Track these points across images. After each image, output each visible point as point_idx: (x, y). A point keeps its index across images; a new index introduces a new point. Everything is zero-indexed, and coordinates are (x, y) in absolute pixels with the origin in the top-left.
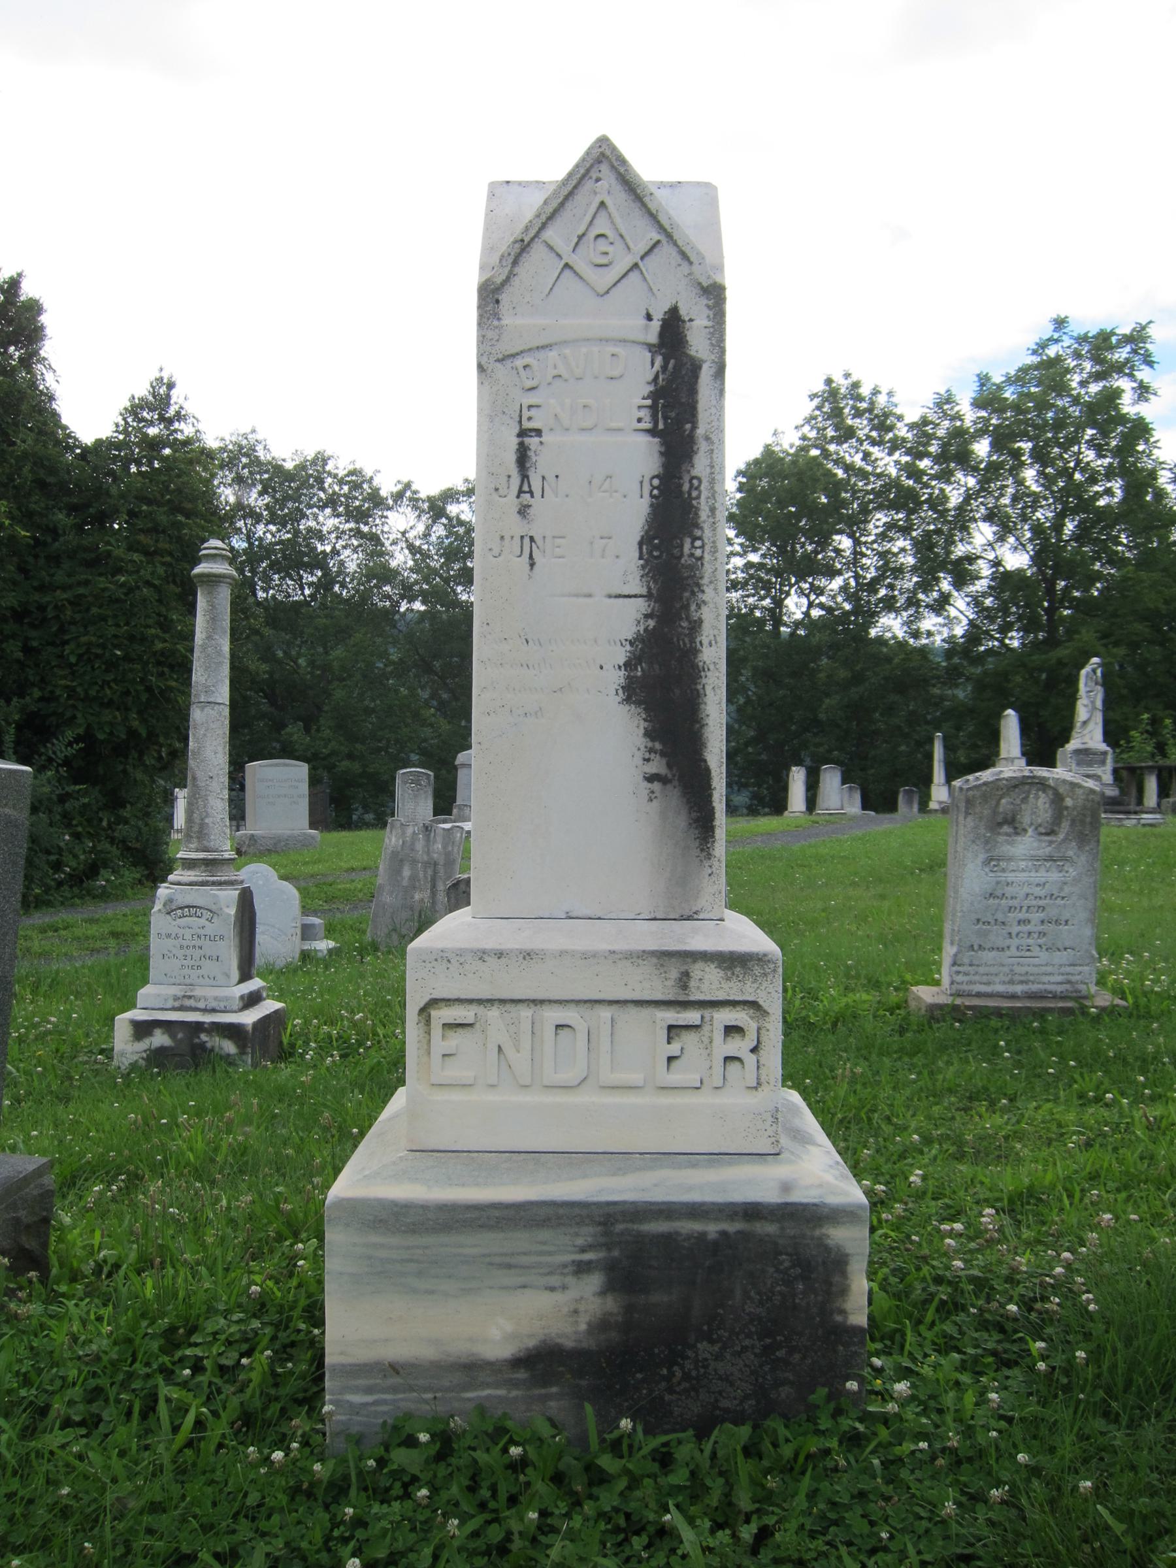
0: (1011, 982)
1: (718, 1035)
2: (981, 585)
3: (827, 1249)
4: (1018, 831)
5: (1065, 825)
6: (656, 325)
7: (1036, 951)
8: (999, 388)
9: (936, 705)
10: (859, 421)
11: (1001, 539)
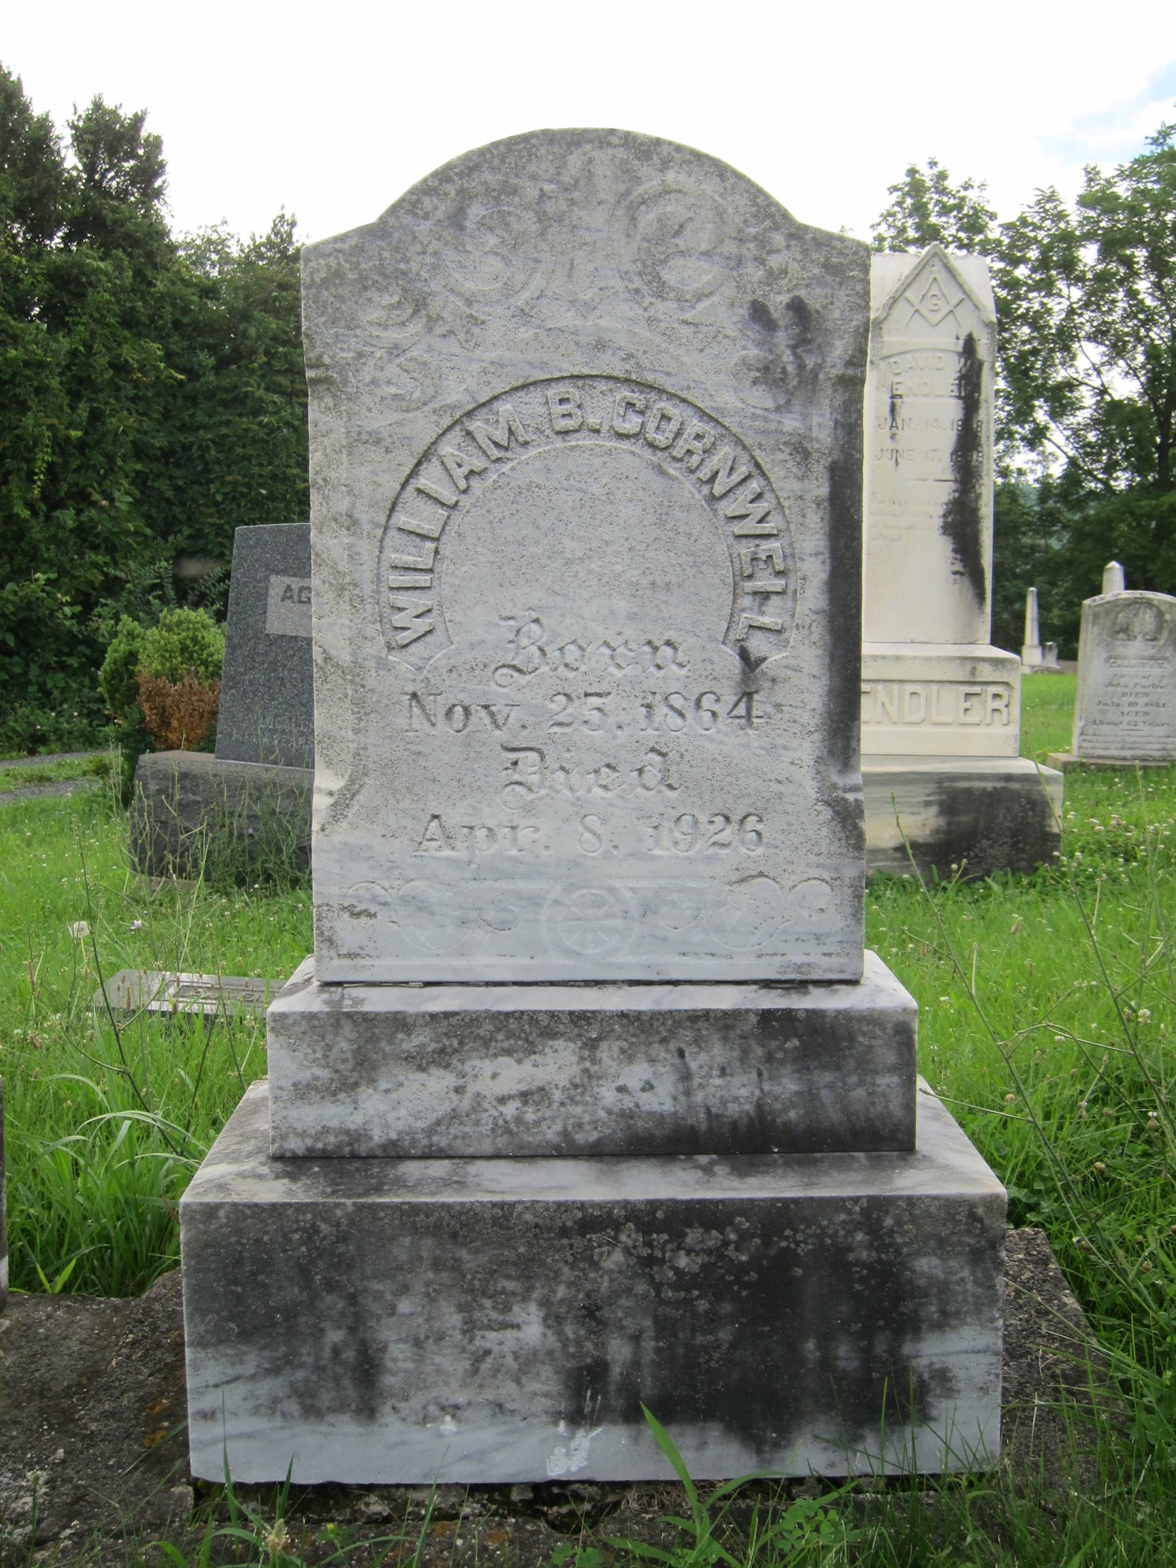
0: (1123, 748)
1: (989, 698)
2: (1082, 416)
3: (1043, 796)
4: (1131, 638)
5: (1165, 634)
6: (961, 342)
7: (1141, 726)
8: (1109, 183)
9: (1026, 556)
10: (944, 219)
11: (1111, 363)
